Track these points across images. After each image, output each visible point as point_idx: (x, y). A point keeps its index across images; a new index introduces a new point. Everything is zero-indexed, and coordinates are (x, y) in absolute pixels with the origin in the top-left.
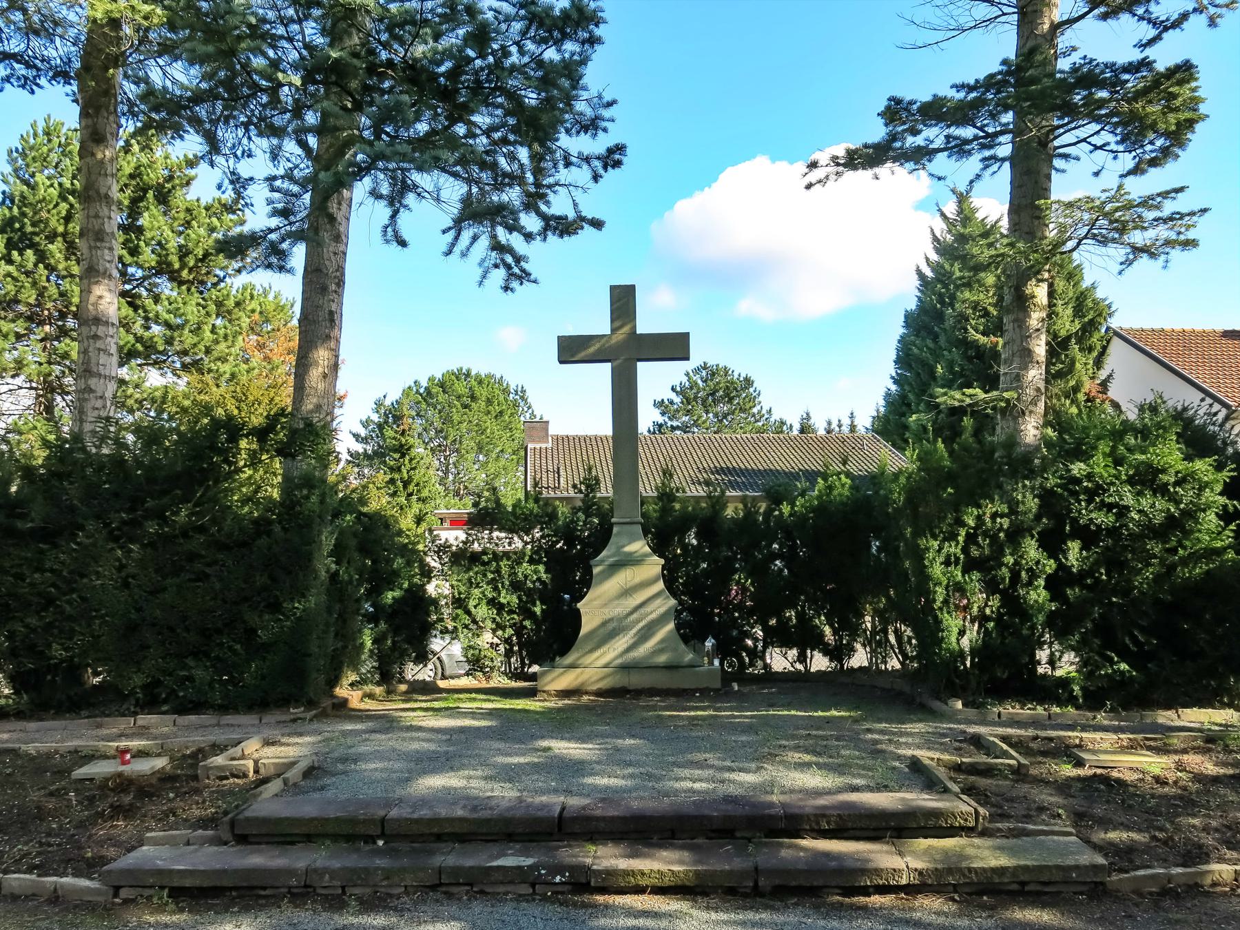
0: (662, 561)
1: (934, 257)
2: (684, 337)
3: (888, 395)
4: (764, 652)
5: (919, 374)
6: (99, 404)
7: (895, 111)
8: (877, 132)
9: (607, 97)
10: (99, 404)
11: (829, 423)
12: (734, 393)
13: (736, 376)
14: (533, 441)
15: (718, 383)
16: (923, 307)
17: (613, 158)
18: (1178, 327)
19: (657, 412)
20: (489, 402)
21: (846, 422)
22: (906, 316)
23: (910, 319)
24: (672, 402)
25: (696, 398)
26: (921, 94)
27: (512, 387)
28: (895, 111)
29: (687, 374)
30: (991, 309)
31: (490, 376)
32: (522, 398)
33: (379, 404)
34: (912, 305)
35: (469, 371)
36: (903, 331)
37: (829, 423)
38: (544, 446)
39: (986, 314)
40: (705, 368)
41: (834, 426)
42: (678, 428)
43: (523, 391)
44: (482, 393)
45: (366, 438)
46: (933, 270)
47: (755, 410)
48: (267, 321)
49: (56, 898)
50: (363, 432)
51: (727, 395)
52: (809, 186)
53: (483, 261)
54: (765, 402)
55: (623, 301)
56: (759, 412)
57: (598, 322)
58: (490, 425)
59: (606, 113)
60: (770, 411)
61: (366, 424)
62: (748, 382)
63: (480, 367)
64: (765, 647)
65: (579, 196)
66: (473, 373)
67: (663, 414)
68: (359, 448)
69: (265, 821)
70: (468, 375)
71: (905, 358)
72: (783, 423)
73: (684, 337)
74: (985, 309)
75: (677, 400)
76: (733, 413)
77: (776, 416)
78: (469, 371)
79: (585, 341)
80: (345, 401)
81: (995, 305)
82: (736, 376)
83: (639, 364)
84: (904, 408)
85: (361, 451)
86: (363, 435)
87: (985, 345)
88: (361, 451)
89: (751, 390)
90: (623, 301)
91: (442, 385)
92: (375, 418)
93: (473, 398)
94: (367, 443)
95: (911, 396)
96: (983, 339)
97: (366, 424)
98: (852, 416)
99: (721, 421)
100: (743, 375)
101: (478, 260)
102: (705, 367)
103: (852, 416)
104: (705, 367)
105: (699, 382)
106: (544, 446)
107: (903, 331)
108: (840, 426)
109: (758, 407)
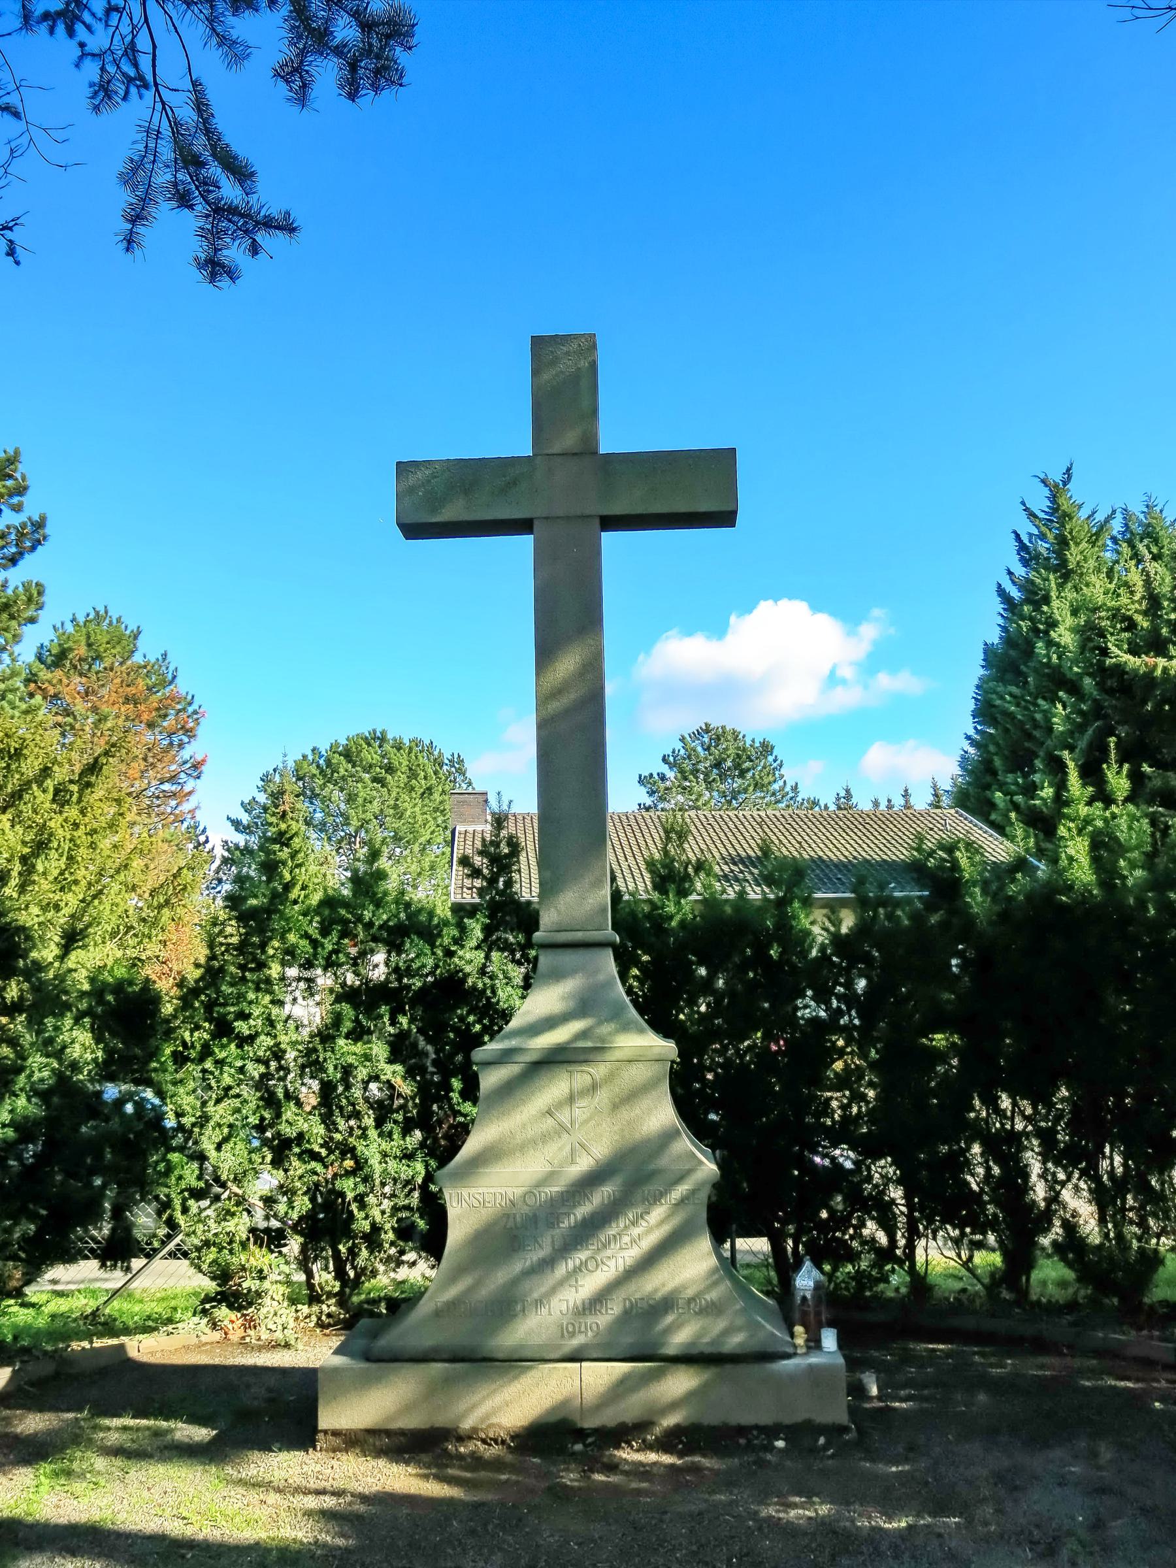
0: (667, 1048)
1: (1020, 571)
2: (721, 462)
3: (964, 760)
4: (911, 1247)
5: (1007, 730)
12: (747, 764)
13: (748, 742)
14: (464, 821)
15: (726, 749)
16: (1009, 640)
19: (643, 791)
20: (413, 775)
22: (985, 652)
23: (991, 656)
24: (663, 778)
25: (695, 772)
27: (447, 755)
29: (683, 739)
30: (1139, 618)
31: (416, 742)
33: (266, 779)
34: (994, 637)
35: (383, 733)
36: (982, 672)
38: (479, 828)
39: (1131, 626)
40: (707, 731)
43: (461, 761)
44: (401, 761)
45: (248, 827)
46: (1021, 588)
47: (776, 786)
48: (99, 657)
50: (245, 818)
51: (737, 766)
53: (136, 166)
54: (790, 774)
55: (564, 379)
56: (782, 789)
57: (502, 429)
58: (412, 807)
60: (795, 788)
61: (247, 807)
62: (766, 748)
63: (401, 729)
64: (913, 1234)
66: (390, 736)
67: (651, 793)
68: (240, 839)
70: (383, 739)
71: (986, 711)
73: (721, 462)
74: (1130, 619)
75: (671, 774)
76: (746, 791)
78: (383, 733)
79: (468, 475)
80: (203, 768)
81: (1145, 613)
82: (748, 742)
83: (612, 542)
84: (988, 779)
85: (242, 844)
86: (245, 822)
87: (1135, 671)
88: (242, 844)
89: (771, 758)
90: (564, 379)
91: (347, 755)
92: (262, 798)
93: (390, 769)
94: (251, 833)
95: (998, 762)
96: (1133, 662)
97: (247, 807)
98: (906, 794)
99: (730, 802)
101: (120, 165)
103: (906, 794)
105: (699, 749)
106: (479, 828)
107: (982, 672)
109: (781, 783)
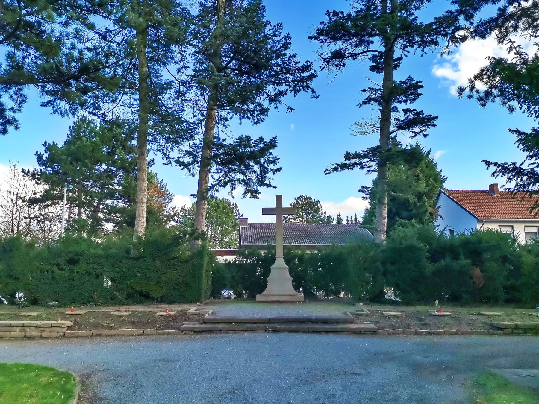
3: (367, 209)
6: (142, 224)
7: (348, 156)
8: (341, 160)
9: (278, 157)
10: (142, 224)
11: (348, 217)
17: (279, 170)
18: (464, 189)
20: (224, 209)
21: (354, 217)
26: (352, 152)
28: (348, 156)
29: (295, 199)
32: (236, 207)
37: (348, 217)
41: (349, 218)
42: (292, 218)
43: (236, 205)
44: (221, 205)
49: (169, 334)
52: (326, 174)
59: (277, 161)
60: (325, 213)
62: (318, 202)
65: (270, 180)
69: (208, 319)
72: (330, 217)
77: (327, 215)
98: (356, 215)
100: (316, 200)
102: (302, 196)
103: (356, 215)
104: (302, 196)
108: (351, 218)
